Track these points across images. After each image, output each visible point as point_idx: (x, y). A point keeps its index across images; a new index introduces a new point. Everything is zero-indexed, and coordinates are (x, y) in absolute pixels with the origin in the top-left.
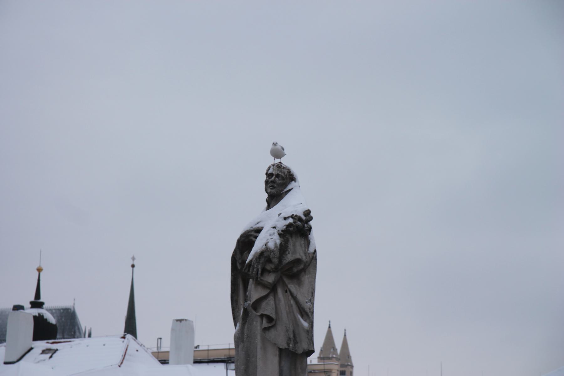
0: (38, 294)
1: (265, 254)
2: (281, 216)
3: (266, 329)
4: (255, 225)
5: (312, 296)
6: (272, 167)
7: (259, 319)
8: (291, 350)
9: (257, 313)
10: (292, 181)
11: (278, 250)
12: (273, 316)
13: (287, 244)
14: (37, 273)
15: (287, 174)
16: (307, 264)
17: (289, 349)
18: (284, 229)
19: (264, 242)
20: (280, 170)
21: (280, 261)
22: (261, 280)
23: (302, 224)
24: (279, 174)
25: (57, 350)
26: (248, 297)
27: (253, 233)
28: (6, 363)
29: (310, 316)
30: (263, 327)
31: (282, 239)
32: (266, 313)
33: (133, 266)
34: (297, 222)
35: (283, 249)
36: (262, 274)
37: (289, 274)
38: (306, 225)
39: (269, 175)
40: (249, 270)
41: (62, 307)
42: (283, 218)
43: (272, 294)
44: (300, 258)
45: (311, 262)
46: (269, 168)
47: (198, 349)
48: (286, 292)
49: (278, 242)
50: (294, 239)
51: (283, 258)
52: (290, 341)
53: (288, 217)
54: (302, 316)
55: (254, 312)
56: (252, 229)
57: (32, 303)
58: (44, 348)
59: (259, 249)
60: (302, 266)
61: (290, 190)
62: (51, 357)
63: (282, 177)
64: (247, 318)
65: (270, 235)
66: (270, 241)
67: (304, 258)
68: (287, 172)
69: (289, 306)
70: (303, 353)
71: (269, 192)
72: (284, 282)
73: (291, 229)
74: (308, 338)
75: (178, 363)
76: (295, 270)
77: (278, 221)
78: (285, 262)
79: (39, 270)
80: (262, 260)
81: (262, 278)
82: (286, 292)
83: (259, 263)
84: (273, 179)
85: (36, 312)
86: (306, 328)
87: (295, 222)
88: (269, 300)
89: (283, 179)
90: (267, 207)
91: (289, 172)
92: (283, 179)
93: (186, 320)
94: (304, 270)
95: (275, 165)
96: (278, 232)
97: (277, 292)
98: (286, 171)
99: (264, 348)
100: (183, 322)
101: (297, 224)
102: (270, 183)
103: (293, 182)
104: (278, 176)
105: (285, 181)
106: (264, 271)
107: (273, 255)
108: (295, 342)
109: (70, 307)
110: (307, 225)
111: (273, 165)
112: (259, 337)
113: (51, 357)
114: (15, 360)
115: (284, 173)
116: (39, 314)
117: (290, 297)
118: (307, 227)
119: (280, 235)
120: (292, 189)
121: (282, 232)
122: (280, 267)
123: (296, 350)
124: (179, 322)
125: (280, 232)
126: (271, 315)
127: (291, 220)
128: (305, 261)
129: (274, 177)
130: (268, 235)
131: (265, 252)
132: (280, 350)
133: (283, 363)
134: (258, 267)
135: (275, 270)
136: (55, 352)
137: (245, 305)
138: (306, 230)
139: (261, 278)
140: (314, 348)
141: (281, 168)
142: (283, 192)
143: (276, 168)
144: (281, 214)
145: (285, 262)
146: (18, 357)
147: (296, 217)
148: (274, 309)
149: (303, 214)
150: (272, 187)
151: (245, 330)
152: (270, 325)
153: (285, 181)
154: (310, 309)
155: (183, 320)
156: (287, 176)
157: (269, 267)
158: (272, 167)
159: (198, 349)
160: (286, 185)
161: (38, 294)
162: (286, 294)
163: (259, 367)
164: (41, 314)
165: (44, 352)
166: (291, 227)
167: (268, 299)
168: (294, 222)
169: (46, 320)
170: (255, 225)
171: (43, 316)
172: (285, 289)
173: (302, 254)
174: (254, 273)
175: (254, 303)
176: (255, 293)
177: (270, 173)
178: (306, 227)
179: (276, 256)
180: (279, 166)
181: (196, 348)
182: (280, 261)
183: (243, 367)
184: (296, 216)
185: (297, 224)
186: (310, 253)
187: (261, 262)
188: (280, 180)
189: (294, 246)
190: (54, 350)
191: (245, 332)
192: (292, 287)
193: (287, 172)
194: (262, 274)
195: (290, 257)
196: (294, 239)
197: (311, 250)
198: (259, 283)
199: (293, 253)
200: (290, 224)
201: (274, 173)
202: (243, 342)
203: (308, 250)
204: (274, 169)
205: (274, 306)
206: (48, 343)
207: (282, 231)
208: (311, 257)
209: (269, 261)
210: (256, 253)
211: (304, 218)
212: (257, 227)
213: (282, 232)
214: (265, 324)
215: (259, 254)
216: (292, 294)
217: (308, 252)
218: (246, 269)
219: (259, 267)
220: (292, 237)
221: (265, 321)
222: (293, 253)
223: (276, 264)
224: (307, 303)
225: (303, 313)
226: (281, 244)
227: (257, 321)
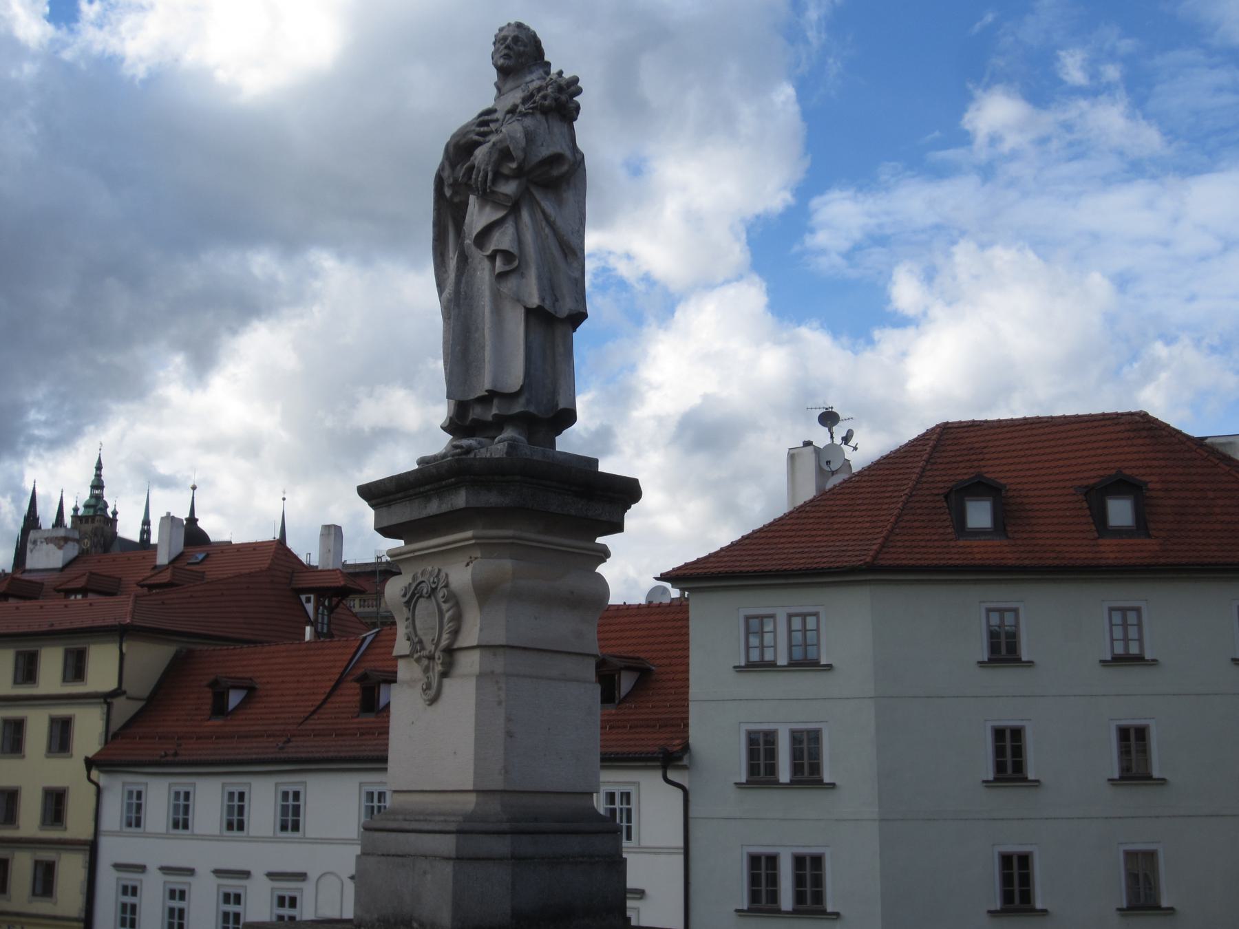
3: (502, 276)
7: (486, 264)
9: (483, 251)
12: (514, 250)
26: (466, 234)
30: (497, 270)
33: (284, 499)
36: (494, 181)
60: (565, 168)
72: (533, 198)
97: (520, 215)
106: (498, 176)
117: (544, 223)
135: (519, 174)
140: (586, 310)
152: (507, 268)
176: (478, 216)
191: (462, 290)
192: (548, 206)
194: (494, 181)
195: (545, 152)
198: (488, 197)
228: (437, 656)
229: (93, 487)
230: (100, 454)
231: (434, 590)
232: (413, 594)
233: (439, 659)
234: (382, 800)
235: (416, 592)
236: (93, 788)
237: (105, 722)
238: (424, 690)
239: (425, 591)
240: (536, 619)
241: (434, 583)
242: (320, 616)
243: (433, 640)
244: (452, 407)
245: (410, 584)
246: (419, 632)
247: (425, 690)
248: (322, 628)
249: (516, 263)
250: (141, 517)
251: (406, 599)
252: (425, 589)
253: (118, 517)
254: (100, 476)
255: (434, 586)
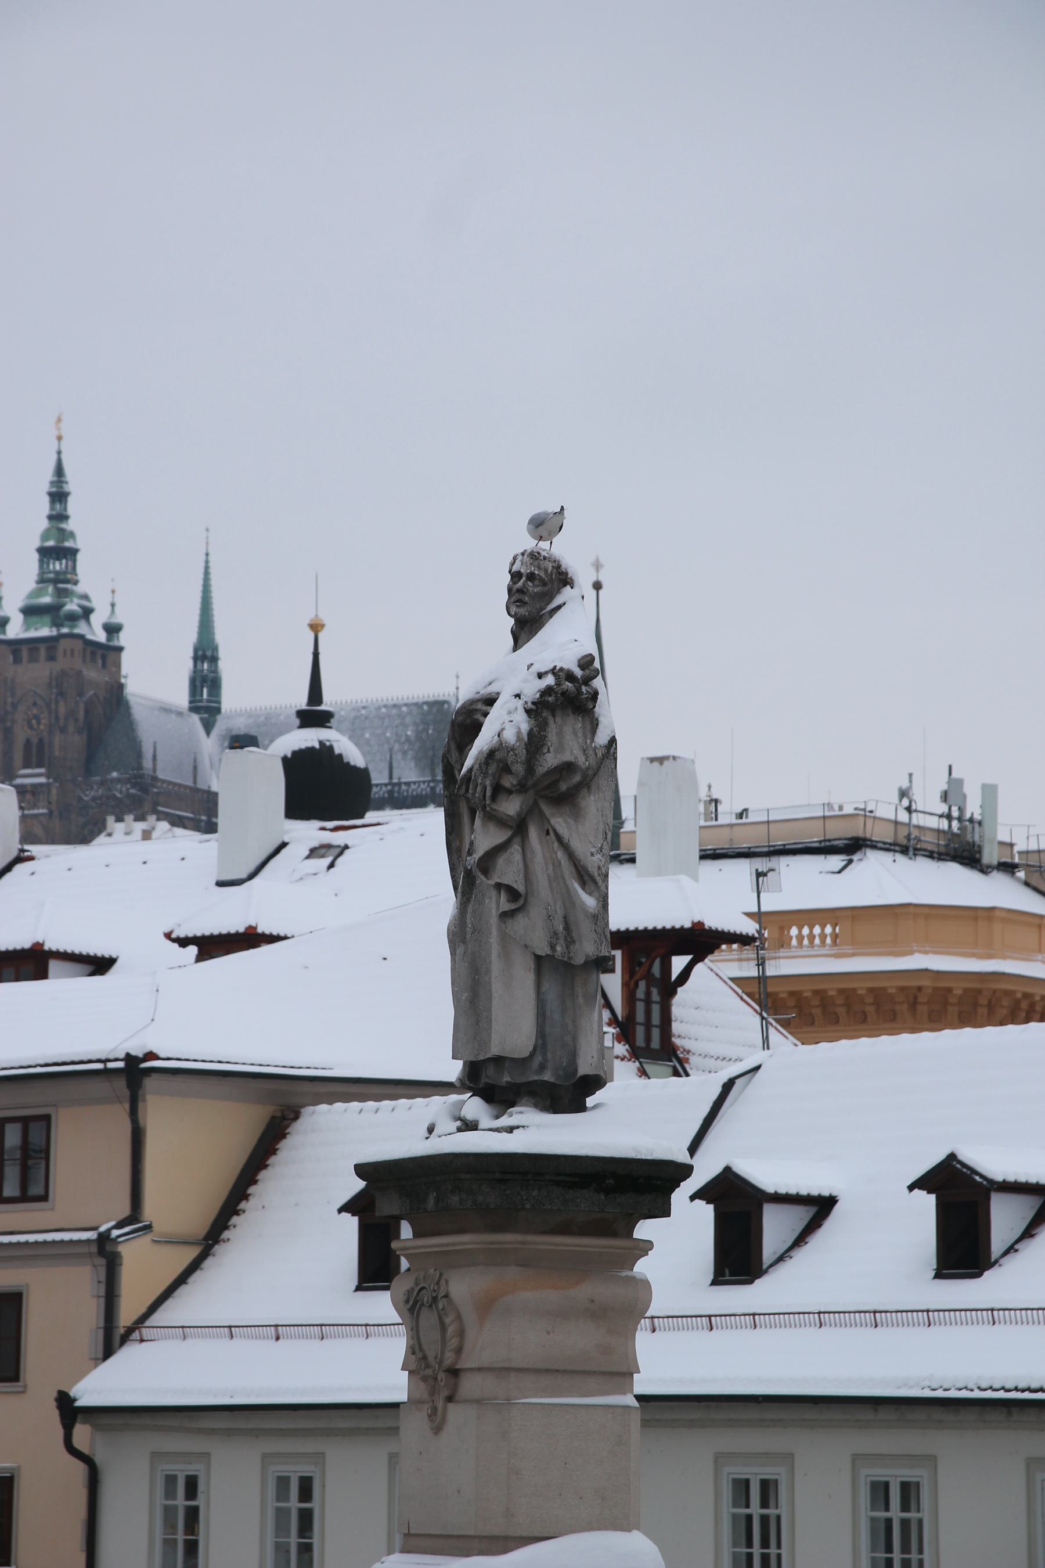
0: (315, 692)
1: (498, 755)
2: (532, 669)
3: (505, 916)
4: (485, 687)
5: (604, 841)
6: (520, 558)
7: (494, 893)
8: (560, 958)
9: (488, 879)
10: (565, 586)
11: (524, 747)
12: (520, 888)
13: (545, 731)
14: (312, 635)
15: (551, 572)
16: (590, 772)
17: (553, 956)
18: (538, 699)
19: (497, 727)
20: (536, 563)
21: (530, 769)
22: (492, 809)
23: (575, 686)
24: (535, 573)
25: (346, 847)
27: (480, 706)
28: (221, 884)
29: (600, 882)
31: (533, 722)
32: (506, 881)
34: (563, 682)
35: (535, 743)
36: (494, 798)
37: (550, 795)
38: (584, 689)
39: (516, 576)
40: (467, 790)
41: (426, 699)
42: (536, 674)
43: (517, 840)
44: (574, 760)
45: (599, 768)
46: (515, 559)
47: (744, 820)
48: (548, 833)
49: (525, 727)
50: (559, 720)
51: (536, 763)
52: (557, 939)
53: (546, 673)
54: (583, 885)
55: (483, 877)
56: (478, 696)
57: (300, 714)
58: (315, 844)
59: (487, 744)
61: (559, 607)
62: (331, 866)
63: (541, 580)
64: (472, 890)
65: (509, 713)
66: (508, 725)
67: (581, 760)
68: (553, 566)
69: (553, 864)
70: (585, 962)
71: (513, 613)
72: (541, 814)
73: (550, 699)
74: (595, 930)
75: (659, 871)
76: (563, 787)
77: (525, 681)
78: (541, 770)
79: (316, 627)
80: (493, 768)
81: (495, 807)
82: (548, 833)
83: (486, 774)
84: (520, 584)
85: (310, 738)
86: (591, 910)
87: (558, 684)
88: (511, 853)
89: (544, 584)
90: (513, 647)
91: (558, 567)
92: (544, 584)
93: (674, 758)
94: (586, 783)
95: (527, 553)
96: (526, 706)
98: (550, 566)
99: (506, 955)
100: (666, 763)
101: (563, 687)
102: (515, 593)
103: (568, 587)
104: (531, 577)
105: (547, 588)
106: (498, 790)
107: (514, 757)
108: (569, 940)
109: (446, 698)
110: (587, 688)
111: (523, 554)
112: (494, 932)
113: (331, 866)
114: (244, 876)
115: (546, 571)
116: (321, 743)
117: (556, 844)
118: (587, 691)
119: (528, 711)
120: (564, 604)
121: (533, 707)
122: (530, 783)
123: (570, 958)
124: (656, 764)
125: (530, 706)
126: (515, 886)
127: (550, 680)
128: (583, 767)
129: (524, 578)
130: (505, 712)
131: (497, 751)
132: (538, 959)
133: (545, 986)
134: (485, 782)
135: (522, 788)
136: (341, 854)
137: (467, 862)
138: (583, 699)
139: (492, 806)
141: (537, 559)
142: (543, 612)
143: (528, 559)
144: (532, 664)
145: (541, 770)
146: (251, 868)
147: (560, 674)
148: (522, 871)
149: (577, 664)
150: (520, 603)
151: (469, 916)
152: (513, 906)
153: (547, 588)
154: (599, 868)
155: (667, 758)
156: (554, 577)
157: (508, 782)
158: (520, 558)
159: (744, 820)
160: (550, 596)
161: (315, 692)
162: (548, 837)
163: (495, 995)
164: (328, 744)
165: (314, 853)
166: (550, 695)
167: (509, 850)
168: (556, 684)
169: (340, 756)
170: (485, 687)
171: (331, 748)
172: (546, 829)
173: (578, 752)
174: (477, 795)
175: (481, 859)
177: (515, 572)
178: (585, 692)
179: (519, 760)
180: (536, 556)
181: (740, 816)
182: (530, 769)
183: (466, 994)
184: (561, 669)
185: (563, 687)
186: (598, 746)
187: (490, 772)
188: (538, 586)
189: (560, 734)
190: (339, 846)
193: (553, 566)
194: (494, 798)
195: (550, 760)
196: (559, 720)
197: (602, 738)
198: (493, 818)
199: (556, 751)
200: (547, 689)
201: (522, 571)
202: (464, 941)
203: (593, 740)
204: (524, 561)
205: (521, 865)
206: (323, 829)
207: (533, 703)
208: (600, 755)
209: (506, 769)
210: (481, 752)
211: (578, 673)
212: (489, 692)
213: (533, 707)
214: (506, 906)
215: (486, 755)
216: (559, 838)
217: (593, 745)
218: (460, 787)
219: (488, 782)
220: (554, 716)
221: (503, 895)
222: (556, 751)
223: (520, 776)
224: (592, 855)
225: (586, 878)
226: (530, 733)
227: (490, 898)
228: (439, 1378)
229: (45, 553)
230: (59, 453)
231: (435, 1299)
232: (416, 1302)
233: (442, 1381)
234: (772, 1502)
235: (418, 1298)
236: (80, 1469)
237: (102, 1301)
238: (430, 1416)
239: (426, 1299)
240: (548, 1333)
241: (434, 1291)
242: (640, 1007)
243: (436, 1357)
244: (467, 1069)
245: (412, 1288)
246: (424, 1347)
247: (431, 1416)
248: (648, 1038)
249: (521, 902)
250: (191, 636)
251: (409, 1306)
252: (426, 1298)
253: (123, 639)
254: (62, 517)
255: (434, 1295)
